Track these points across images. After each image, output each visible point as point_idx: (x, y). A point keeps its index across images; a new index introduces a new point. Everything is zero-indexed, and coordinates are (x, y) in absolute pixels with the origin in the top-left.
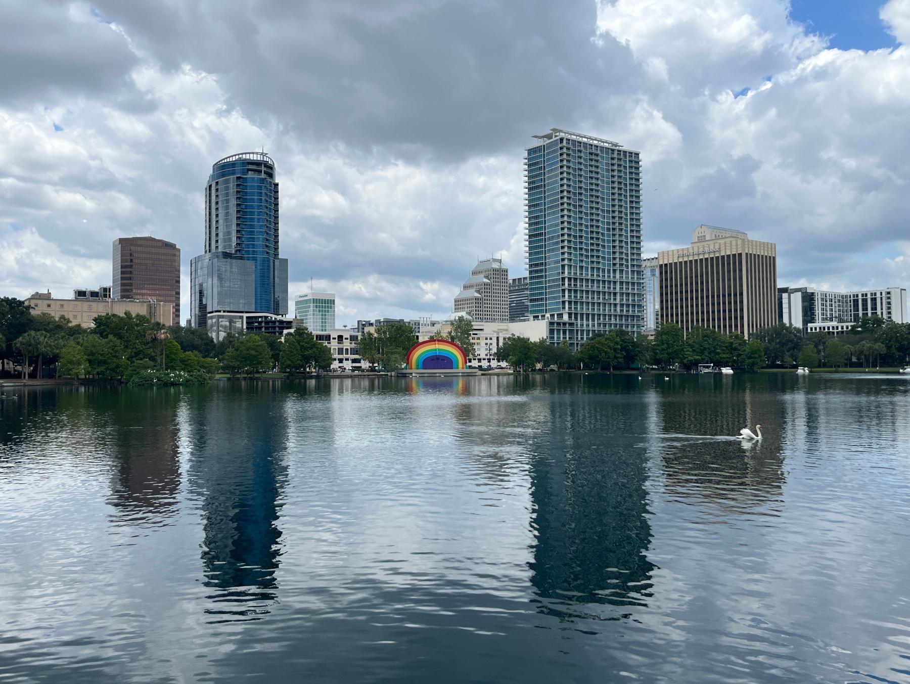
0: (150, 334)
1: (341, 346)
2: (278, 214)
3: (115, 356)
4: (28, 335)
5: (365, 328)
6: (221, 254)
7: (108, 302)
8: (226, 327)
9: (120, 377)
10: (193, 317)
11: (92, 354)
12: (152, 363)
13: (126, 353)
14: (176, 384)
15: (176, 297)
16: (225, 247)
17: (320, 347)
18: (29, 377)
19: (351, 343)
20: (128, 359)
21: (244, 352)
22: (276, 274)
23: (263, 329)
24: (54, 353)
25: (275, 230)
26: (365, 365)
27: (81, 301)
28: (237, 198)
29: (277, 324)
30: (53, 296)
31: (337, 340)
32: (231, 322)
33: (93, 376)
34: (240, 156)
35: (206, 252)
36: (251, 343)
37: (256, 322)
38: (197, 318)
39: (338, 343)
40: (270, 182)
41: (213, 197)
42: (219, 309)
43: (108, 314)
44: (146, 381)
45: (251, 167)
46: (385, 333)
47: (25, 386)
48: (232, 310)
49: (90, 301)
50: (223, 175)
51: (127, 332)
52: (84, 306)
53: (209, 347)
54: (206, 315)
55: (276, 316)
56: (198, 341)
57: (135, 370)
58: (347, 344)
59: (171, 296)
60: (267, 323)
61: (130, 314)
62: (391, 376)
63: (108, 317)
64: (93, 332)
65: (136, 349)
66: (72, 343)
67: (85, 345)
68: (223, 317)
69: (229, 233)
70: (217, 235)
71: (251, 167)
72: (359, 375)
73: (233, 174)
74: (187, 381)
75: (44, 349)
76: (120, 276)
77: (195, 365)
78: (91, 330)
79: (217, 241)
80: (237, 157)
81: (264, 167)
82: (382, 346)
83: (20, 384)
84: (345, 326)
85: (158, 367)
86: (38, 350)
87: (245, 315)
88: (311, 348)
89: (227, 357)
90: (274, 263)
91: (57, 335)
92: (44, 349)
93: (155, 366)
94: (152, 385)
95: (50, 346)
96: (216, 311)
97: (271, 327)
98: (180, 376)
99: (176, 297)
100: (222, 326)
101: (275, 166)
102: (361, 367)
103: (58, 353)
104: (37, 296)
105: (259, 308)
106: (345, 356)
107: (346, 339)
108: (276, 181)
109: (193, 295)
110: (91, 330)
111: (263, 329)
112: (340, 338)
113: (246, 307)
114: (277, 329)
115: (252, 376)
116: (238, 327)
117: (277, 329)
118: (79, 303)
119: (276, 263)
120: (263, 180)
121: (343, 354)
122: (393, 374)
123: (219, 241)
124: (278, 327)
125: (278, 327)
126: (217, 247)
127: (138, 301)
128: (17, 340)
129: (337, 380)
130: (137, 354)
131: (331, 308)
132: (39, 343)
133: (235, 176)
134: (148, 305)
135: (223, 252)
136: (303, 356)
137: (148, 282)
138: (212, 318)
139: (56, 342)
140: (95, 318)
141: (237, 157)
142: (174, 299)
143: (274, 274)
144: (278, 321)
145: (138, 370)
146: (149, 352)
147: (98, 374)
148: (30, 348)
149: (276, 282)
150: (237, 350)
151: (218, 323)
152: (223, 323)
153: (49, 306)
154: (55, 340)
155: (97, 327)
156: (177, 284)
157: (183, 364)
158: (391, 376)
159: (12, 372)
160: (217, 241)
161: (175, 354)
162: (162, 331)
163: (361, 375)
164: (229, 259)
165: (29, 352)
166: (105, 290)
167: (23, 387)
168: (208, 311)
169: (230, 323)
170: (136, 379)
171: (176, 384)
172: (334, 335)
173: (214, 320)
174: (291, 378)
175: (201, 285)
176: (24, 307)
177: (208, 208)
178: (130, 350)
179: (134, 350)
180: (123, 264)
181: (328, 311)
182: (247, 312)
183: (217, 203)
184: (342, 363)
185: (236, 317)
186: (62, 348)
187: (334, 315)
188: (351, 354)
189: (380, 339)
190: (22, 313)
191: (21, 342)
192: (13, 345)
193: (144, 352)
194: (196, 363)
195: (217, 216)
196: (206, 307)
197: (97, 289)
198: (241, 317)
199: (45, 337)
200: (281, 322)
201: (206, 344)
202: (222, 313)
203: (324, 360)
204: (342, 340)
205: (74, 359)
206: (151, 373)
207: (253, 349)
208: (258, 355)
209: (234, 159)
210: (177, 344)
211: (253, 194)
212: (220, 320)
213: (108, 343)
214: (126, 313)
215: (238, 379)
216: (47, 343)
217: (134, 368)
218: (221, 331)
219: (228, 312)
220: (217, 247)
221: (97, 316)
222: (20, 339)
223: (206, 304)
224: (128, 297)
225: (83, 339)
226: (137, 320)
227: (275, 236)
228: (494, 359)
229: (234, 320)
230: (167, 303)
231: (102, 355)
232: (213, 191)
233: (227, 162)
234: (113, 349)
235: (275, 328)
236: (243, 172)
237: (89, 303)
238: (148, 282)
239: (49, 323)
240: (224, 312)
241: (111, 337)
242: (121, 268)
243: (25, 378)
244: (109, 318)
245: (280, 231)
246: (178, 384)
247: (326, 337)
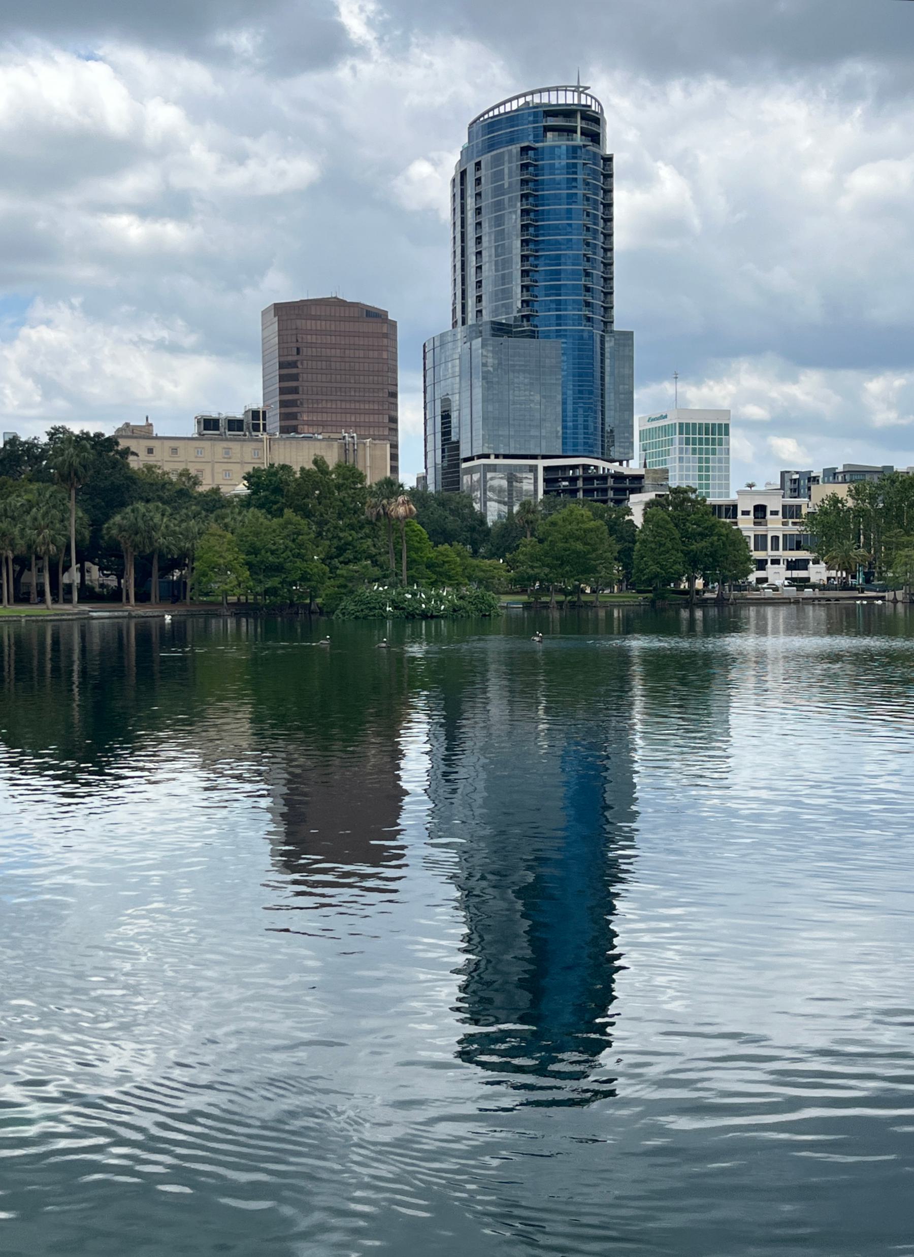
0: (375, 506)
1: (761, 530)
2: (611, 228)
3: (298, 556)
4: (133, 511)
5: (814, 487)
6: (488, 327)
7: (261, 440)
8: (500, 490)
9: (308, 601)
10: (431, 471)
11: (254, 551)
12: (377, 571)
13: (320, 548)
14: (432, 617)
15: (390, 429)
16: (495, 311)
17: (724, 531)
18: (136, 600)
19: (784, 524)
20: (323, 561)
21: (560, 545)
22: (607, 369)
23: (580, 495)
24: (180, 549)
25: (605, 265)
26: (818, 573)
27: (211, 439)
28: (522, 195)
29: (611, 482)
30: (158, 431)
31: (752, 516)
32: (511, 479)
33: (255, 599)
34: (529, 98)
35: (455, 324)
36: (574, 526)
37: (564, 479)
38: (440, 472)
39: (755, 523)
40: (595, 155)
41: (470, 203)
42: (486, 452)
43: (272, 466)
44: (371, 609)
45: (551, 122)
46: (873, 498)
47: (130, 617)
48: (513, 452)
49: (227, 440)
50: (491, 146)
51: (320, 503)
52: (215, 449)
53: (476, 536)
54: (458, 466)
55: (607, 465)
56: (455, 521)
57: (345, 586)
58: (775, 526)
59: (378, 425)
60: (588, 479)
61: (324, 462)
62: (895, 601)
63: (273, 471)
64: (246, 503)
65: (340, 539)
66: (214, 527)
67: (239, 531)
68: (493, 468)
69: (504, 279)
70: (479, 284)
71: (551, 122)
72: (814, 599)
73: (511, 141)
74: (455, 611)
75: (161, 540)
76: (277, 386)
77: (457, 574)
78: (241, 500)
79: (479, 299)
80: (522, 101)
81: (582, 118)
82: (865, 530)
83: (121, 614)
84: (751, 486)
85: (392, 579)
86: (151, 544)
87: (541, 463)
88: (703, 536)
89: (521, 557)
90: (603, 343)
91: (184, 511)
92: (161, 540)
93: (385, 576)
94: (383, 618)
95: (174, 533)
96: (480, 457)
97: (597, 490)
98: (440, 598)
99: (390, 429)
100: (492, 489)
101: (605, 115)
102: (808, 579)
103: (188, 550)
104: (128, 431)
105: (570, 447)
106: (770, 552)
107: (775, 513)
108: (608, 152)
109: (430, 423)
110: (241, 500)
111: (580, 495)
112: (760, 510)
113: (512, 445)
114: (611, 494)
115: (576, 599)
116: (527, 491)
117: (611, 494)
118: (206, 444)
119: (607, 345)
120: (574, 151)
121: (766, 549)
122: (900, 595)
123: (484, 297)
124: (612, 489)
125: (612, 489)
126: (479, 312)
127: (320, 437)
128: (111, 521)
129: (751, 608)
130: (341, 550)
131: (720, 444)
132: (155, 528)
133: (519, 146)
134: (340, 447)
135: (493, 323)
136: (686, 554)
137: (329, 397)
138: (470, 471)
139: (184, 525)
140: (248, 473)
141: (522, 101)
142: (386, 433)
143: (603, 368)
144: (613, 476)
145: (350, 585)
146: (365, 546)
147: (267, 592)
148: (138, 538)
149: (607, 386)
150: (541, 541)
151: (485, 482)
152: (495, 483)
153: (150, 451)
154: (182, 521)
155: (253, 493)
156: (392, 400)
157: (434, 572)
158: (895, 601)
159: (97, 589)
160: (479, 299)
161: (417, 550)
162: (400, 499)
163: (819, 599)
164: (505, 338)
165: (136, 546)
166: (255, 414)
167: (126, 620)
168: (462, 456)
169: (510, 483)
170: (348, 604)
171: (432, 617)
172: (746, 504)
173: (476, 477)
174: (659, 603)
175: (446, 402)
176: (117, 452)
177: (458, 223)
178: (328, 542)
179: (335, 541)
180: (282, 359)
181: (714, 450)
182: (544, 457)
183: (478, 211)
184: (764, 569)
185: (521, 468)
186: (195, 538)
187: (727, 460)
188: (785, 549)
189: (859, 513)
190: (115, 464)
191: (120, 526)
192: (105, 532)
193: (354, 547)
194: (459, 569)
195: (479, 240)
196: (458, 448)
197: (239, 414)
198: (533, 469)
199: (163, 515)
200: (619, 477)
201: (472, 529)
202: (492, 461)
203: (735, 564)
204: (764, 517)
205: (221, 561)
206: (381, 592)
207: (578, 539)
208: (589, 553)
209: (515, 107)
210: (420, 527)
211: (555, 184)
212: (489, 475)
213: (284, 526)
214: (315, 462)
215: (546, 606)
216: (167, 527)
217: (341, 581)
218: (491, 500)
219: (506, 457)
220: (479, 312)
221: (251, 470)
222: (118, 518)
223: (458, 442)
224: (295, 429)
225: (234, 519)
226: (338, 475)
227: (605, 279)
228: (816, 562)
229: (518, 475)
230: (377, 442)
231: (273, 552)
232: (470, 191)
233: (500, 115)
234: (294, 541)
235: (604, 491)
236: (536, 136)
237: (225, 444)
238: (329, 397)
239: (163, 486)
240: (497, 457)
241: (288, 513)
242: (280, 368)
243: (128, 598)
244: (275, 474)
245: (616, 268)
246: (437, 617)
247: (727, 510)
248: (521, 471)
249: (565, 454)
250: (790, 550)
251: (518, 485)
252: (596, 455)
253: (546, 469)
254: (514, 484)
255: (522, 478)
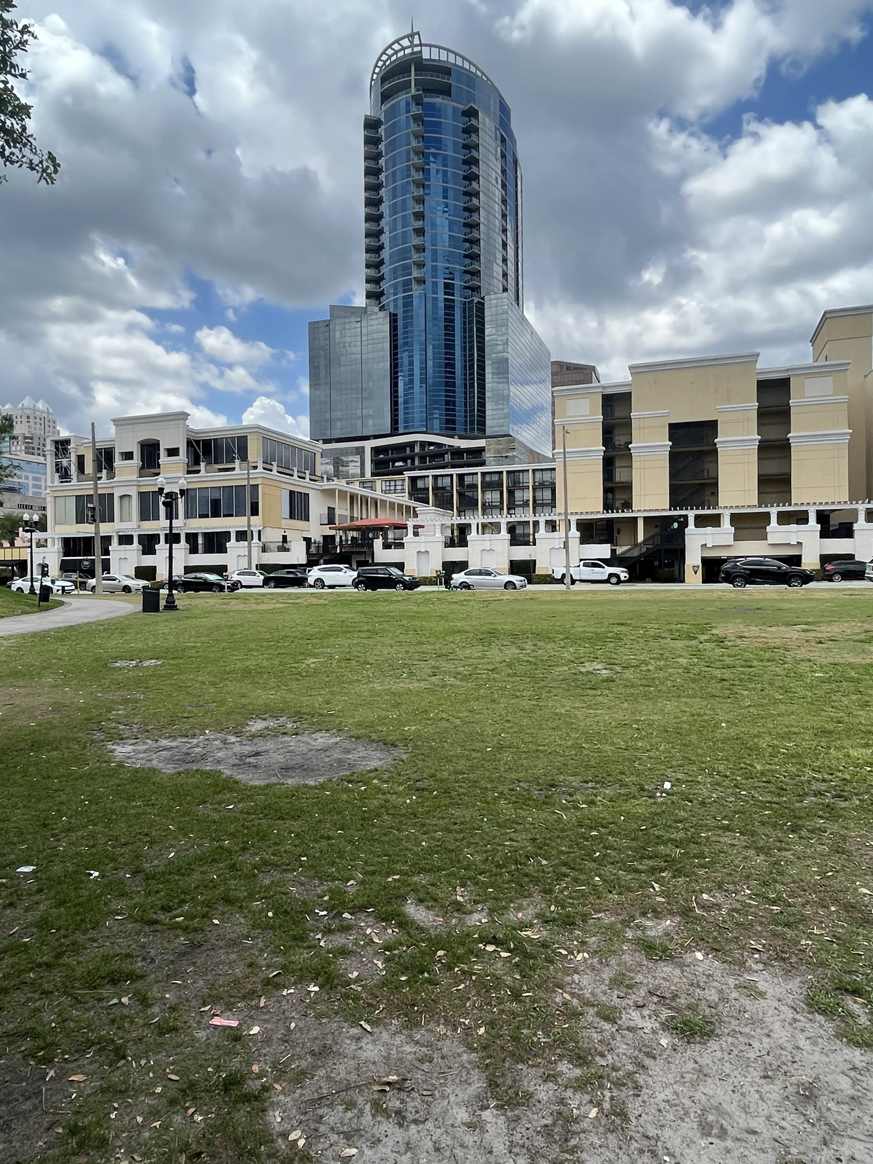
87: (369, 445)
107: (173, 452)
185: (347, 452)
229: (344, 459)
248: (347, 455)
249: (407, 431)
250: (201, 516)
251: (344, 468)
252: (435, 432)
253: (376, 451)
254: (341, 468)
255: (348, 462)
